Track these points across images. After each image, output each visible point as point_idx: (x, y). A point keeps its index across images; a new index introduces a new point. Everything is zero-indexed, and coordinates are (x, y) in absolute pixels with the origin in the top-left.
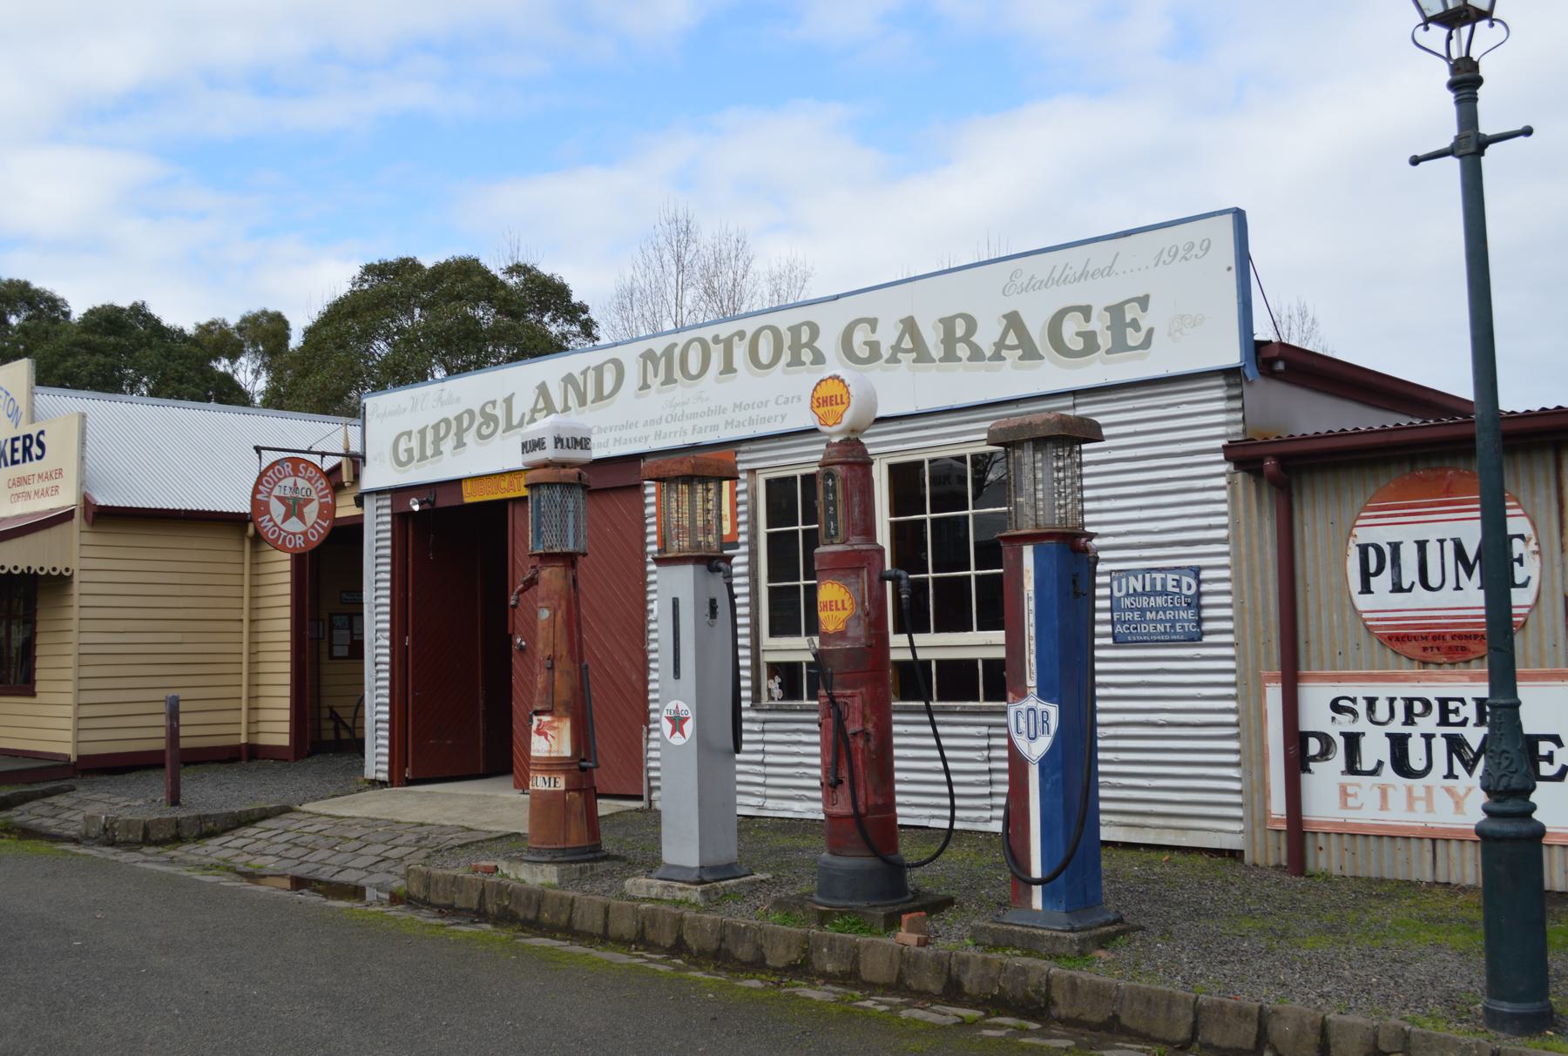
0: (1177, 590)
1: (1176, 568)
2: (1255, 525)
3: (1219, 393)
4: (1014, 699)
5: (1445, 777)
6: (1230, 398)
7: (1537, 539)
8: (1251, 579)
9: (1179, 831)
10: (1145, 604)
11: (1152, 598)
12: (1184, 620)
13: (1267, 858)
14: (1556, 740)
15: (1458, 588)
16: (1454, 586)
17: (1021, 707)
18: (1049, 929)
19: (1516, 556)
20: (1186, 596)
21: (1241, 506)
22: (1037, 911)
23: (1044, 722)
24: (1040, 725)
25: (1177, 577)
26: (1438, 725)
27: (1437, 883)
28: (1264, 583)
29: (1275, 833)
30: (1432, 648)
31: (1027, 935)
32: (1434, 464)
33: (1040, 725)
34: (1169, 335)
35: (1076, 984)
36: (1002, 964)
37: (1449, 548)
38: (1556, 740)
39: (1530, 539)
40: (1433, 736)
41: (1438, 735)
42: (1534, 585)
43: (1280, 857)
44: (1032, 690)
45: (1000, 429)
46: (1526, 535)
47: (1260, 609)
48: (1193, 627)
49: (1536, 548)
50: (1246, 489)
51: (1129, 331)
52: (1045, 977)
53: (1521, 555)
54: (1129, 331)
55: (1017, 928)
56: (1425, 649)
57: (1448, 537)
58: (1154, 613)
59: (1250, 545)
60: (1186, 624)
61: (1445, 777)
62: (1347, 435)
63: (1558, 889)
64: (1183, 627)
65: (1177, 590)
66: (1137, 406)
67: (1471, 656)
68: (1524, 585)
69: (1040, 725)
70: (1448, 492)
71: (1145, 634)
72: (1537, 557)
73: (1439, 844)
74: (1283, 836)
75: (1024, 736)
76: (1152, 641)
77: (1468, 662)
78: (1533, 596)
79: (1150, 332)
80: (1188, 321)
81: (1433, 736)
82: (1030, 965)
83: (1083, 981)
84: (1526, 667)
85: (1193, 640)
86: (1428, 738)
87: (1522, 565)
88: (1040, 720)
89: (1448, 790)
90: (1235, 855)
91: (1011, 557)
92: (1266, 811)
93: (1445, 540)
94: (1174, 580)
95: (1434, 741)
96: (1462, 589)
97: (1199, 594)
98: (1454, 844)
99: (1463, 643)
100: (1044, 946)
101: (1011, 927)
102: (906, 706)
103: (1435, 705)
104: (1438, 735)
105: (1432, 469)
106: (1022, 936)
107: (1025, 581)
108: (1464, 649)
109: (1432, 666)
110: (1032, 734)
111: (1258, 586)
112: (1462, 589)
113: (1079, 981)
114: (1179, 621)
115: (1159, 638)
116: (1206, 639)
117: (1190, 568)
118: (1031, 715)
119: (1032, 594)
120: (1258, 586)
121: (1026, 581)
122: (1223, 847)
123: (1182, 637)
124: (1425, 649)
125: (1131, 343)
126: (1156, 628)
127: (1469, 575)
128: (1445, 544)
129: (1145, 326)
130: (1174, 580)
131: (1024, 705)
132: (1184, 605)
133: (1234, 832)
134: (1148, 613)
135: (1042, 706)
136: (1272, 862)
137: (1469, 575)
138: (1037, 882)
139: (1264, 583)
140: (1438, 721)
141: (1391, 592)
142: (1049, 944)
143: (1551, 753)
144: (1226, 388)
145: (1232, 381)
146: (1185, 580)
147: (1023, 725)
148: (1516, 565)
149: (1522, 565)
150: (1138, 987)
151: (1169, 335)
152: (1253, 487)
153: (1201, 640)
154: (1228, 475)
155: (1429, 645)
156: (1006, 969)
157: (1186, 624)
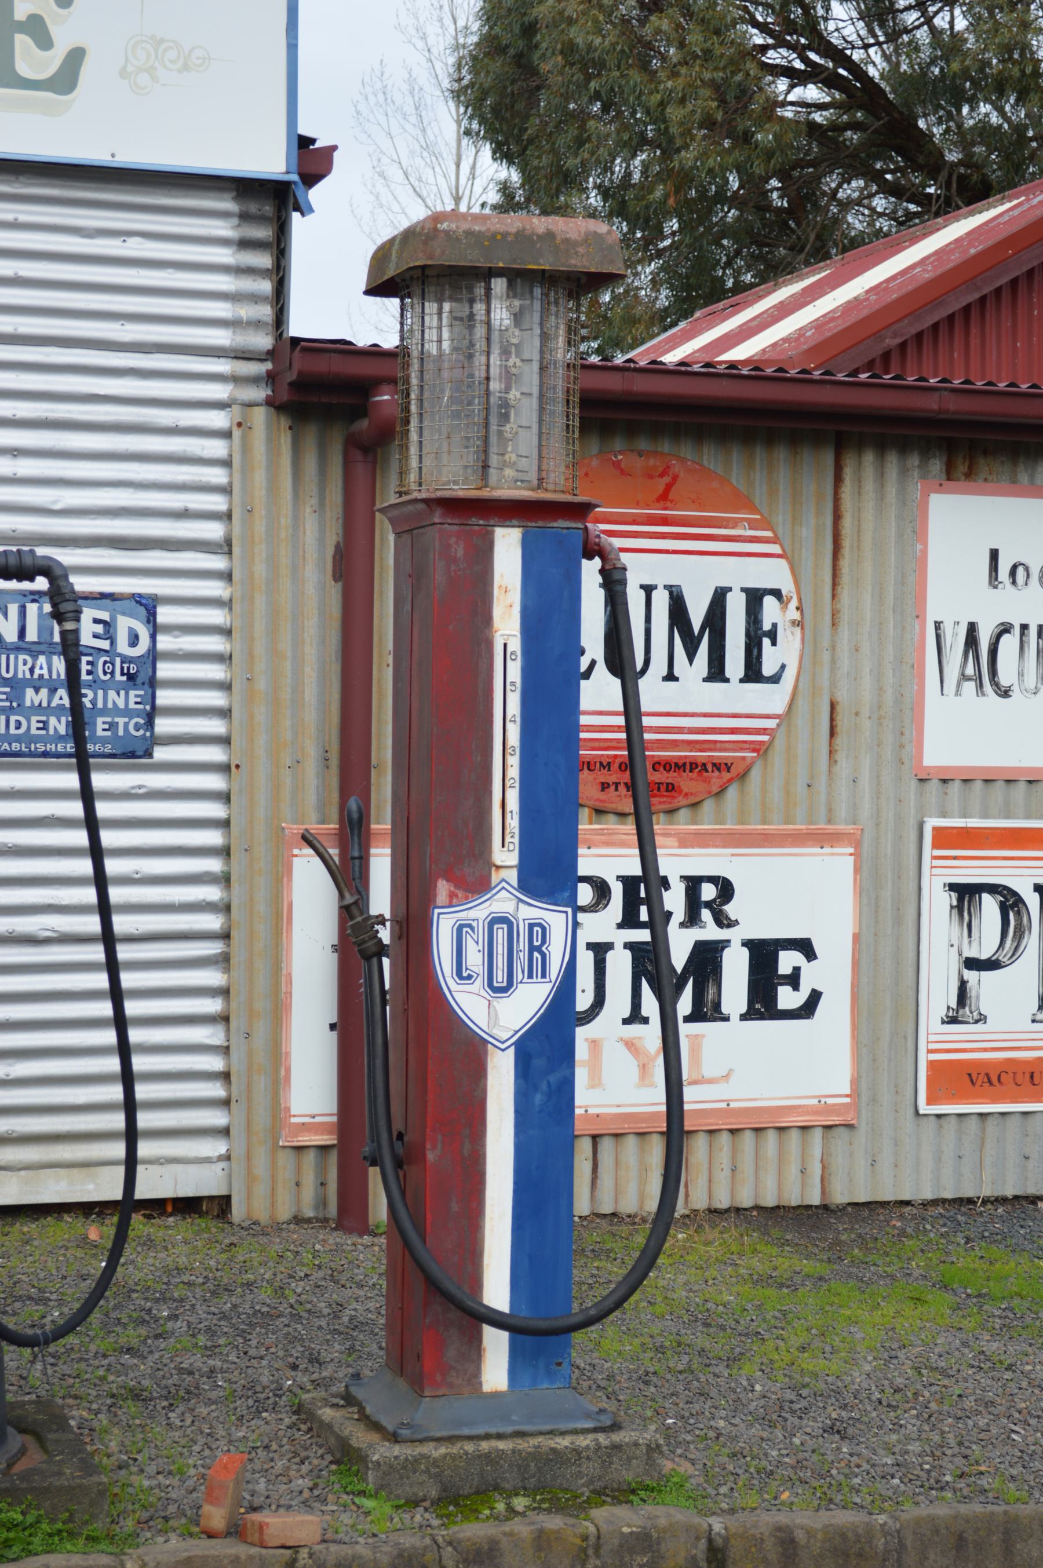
0: (105, 645)
1: (103, 596)
2: (285, 520)
3: (223, 229)
4: (452, 895)
5: (626, 1022)
6: (244, 244)
7: (800, 600)
8: (273, 631)
9: (75, 1171)
10: (23, 671)
11: (42, 659)
12: (116, 711)
13: (273, 1204)
14: (805, 947)
15: (670, 677)
16: (665, 673)
17: (472, 914)
18: (563, 1433)
19: (767, 626)
20: (125, 659)
21: (260, 477)
22: (496, 1395)
23: (532, 949)
24: (522, 957)
25: (105, 616)
26: (620, 926)
27: (598, 1215)
28: (297, 644)
29: (291, 1153)
30: (617, 785)
31: (535, 1455)
32: (643, 444)
33: (522, 957)
34: (123, 73)
35: (793, 1541)
36: (585, 1538)
37: (661, 601)
38: (805, 947)
39: (790, 599)
40: (609, 946)
41: (619, 946)
42: (789, 678)
43: (298, 1202)
44: (504, 874)
45: (469, 233)
46: (784, 593)
47: (286, 695)
48: (137, 727)
49: (796, 616)
50: (271, 442)
51: (22, 42)
52: (703, 1544)
53: (775, 626)
54: (22, 42)
55: (501, 1445)
56: (604, 786)
57: (660, 582)
58: (44, 692)
59: (272, 561)
60: (121, 721)
61: (626, 1022)
62: (635, 370)
63: (794, 1204)
64: (112, 726)
65: (105, 645)
66: (23, 218)
67: (682, 801)
68: (775, 679)
69: (524, 956)
70: (664, 498)
71: (18, 739)
72: (798, 631)
73: (606, 1146)
74: (333, 1158)
75: (479, 985)
76: (31, 754)
77: (671, 812)
78: (787, 698)
79: (76, 57)
80: (172, 54)
81: (609, 946)
82: (663, 1522)
83: (810, 1533)
84: (764, 823)
85: (133, 755)
86: (600, 950)
87: (774, 643)
88: (523, 944)
89: (630, 1045)
90: (222, 1204)
91: (460, 553)
92: (278, 1110)
93: (655, 587)
94: (96, 621)
95: (610, 956)
96: (677, 679)
97: (153, 656)
98: (631, 1142)
99: (671, 777)
100: (579, 1475)
101: (485, 1445)
102: (282, 919)
103: (617, 890)
104: (619, 946)
105: (640, 454)
106: (521, 1462)
107: (497, 612)
108: (671, 788)
109: (611, 818)
110: (500, 977)
111: (285, 646)
112: (677, 679)
113: (800, 1536)
114: (104, 711)
115: (51, 747)
116: (161, 754)
117: (138, 599)
118: (501, 934)
119: (515, 645)
120: (285, 646)
121: (498, 611)
122: (198, 1195)
123: (108, 749)
124: (604, 786)
125: (23, 69)
126: (45, 726)
127: (691, 656)
128: (654, 594)
129: (63, 41)
130: (96, 621)
131: (479, 912)
132: (118, 677)
133: (207, 1160)
134: (30, 692)
135: (529, 912)
136: (284, 1213)
137: (691, 656)
138: (497, 1320)
139: (297, 644)
140: (619, 919)
141: (704, 680)
142: (590, 1468)
143: (797, 970)
144: (235, 221)
145: (253, 208)
146: (124, 624)
147: (474, 958)
148: (766, 642)
149: (774, 643)
150: (932, 1519)
151: (123, 73)
152: (285, 440)
153: (149, 754)
154: (236, 408)
155: (612, 779)
156: (597, 1547)
157: (121, 721)
